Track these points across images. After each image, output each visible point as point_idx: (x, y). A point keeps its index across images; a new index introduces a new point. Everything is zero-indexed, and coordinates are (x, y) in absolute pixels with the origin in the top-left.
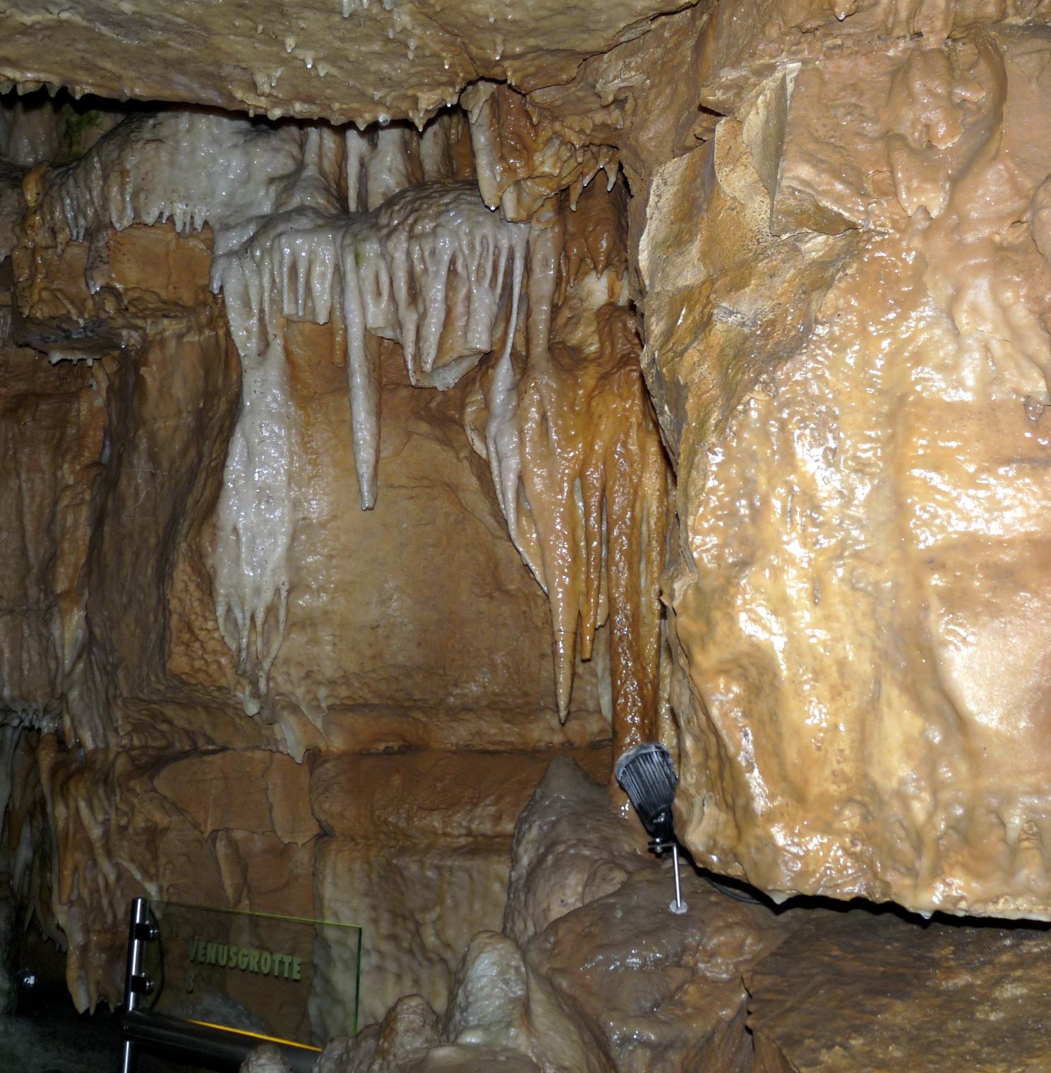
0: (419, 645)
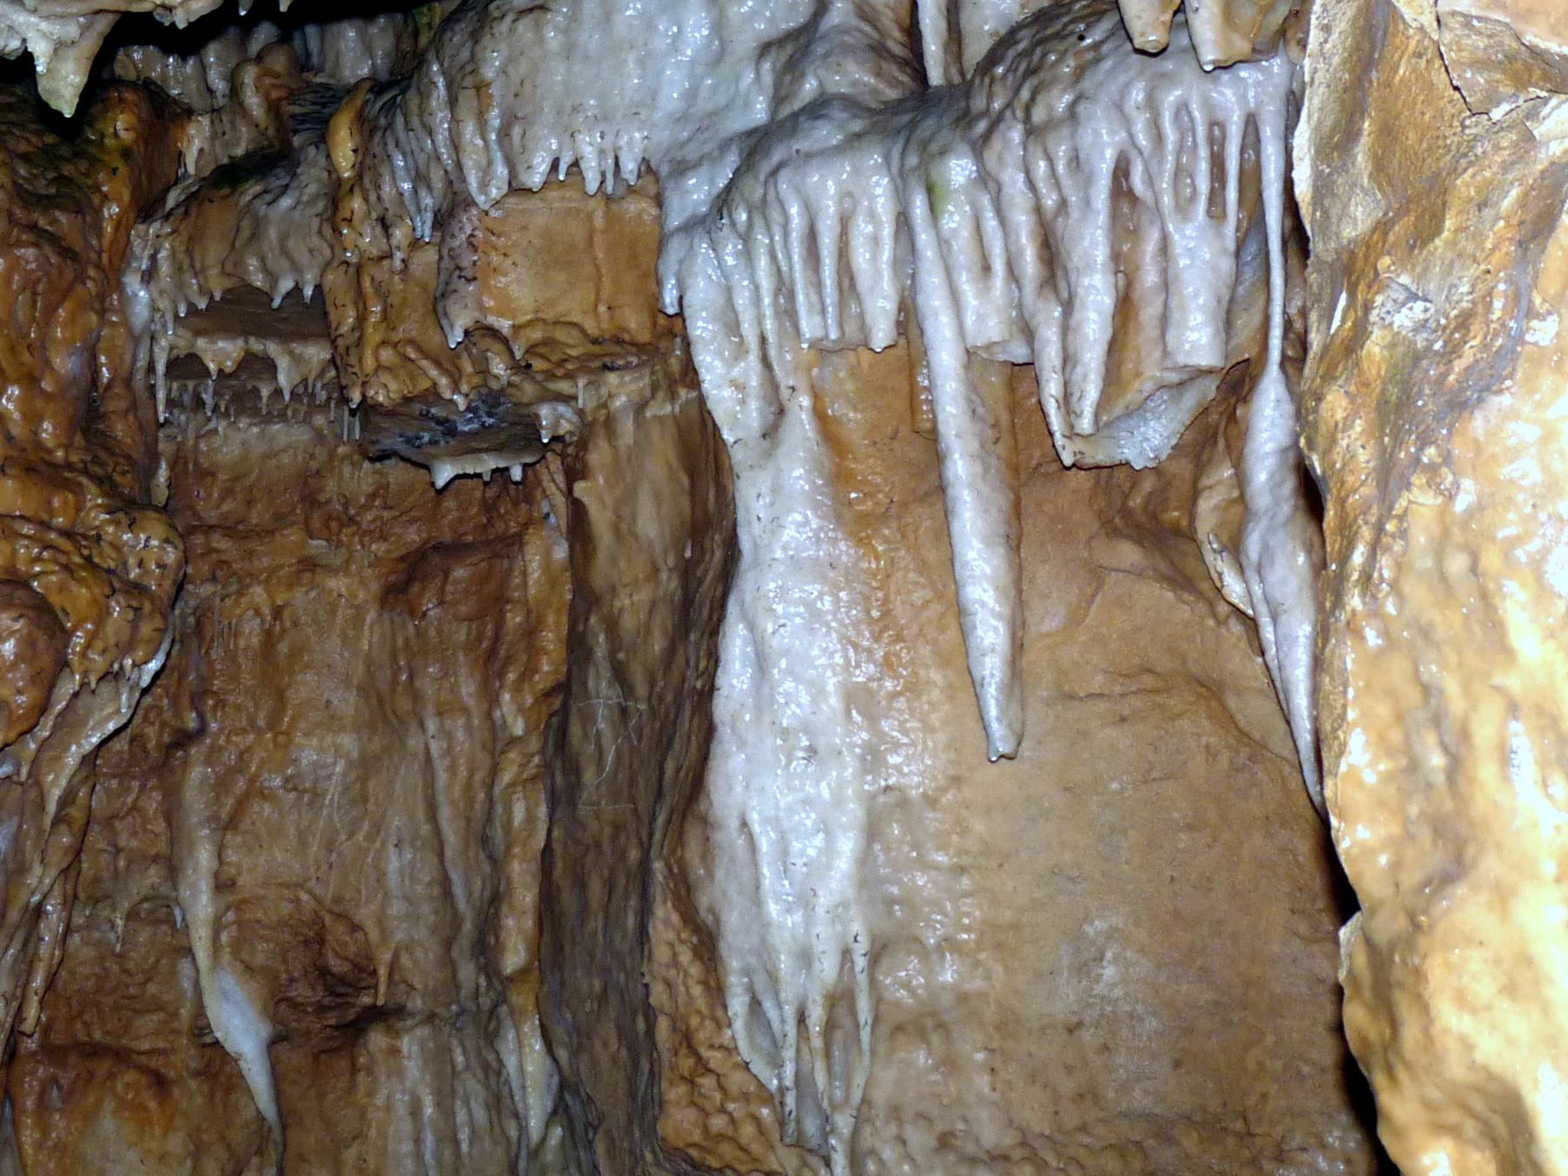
0: (1177, 1064)
